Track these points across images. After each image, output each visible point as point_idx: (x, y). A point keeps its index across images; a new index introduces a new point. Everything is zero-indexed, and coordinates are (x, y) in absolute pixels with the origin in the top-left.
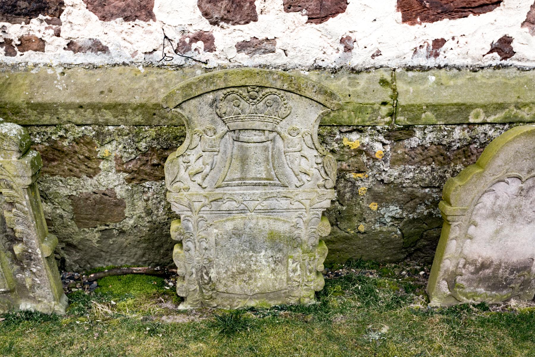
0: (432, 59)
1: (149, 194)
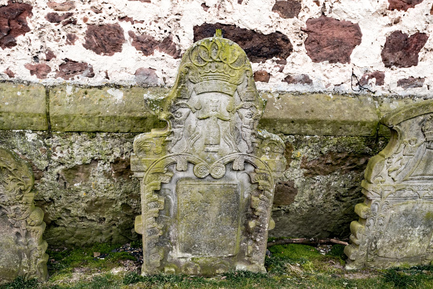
1: (316, 185)
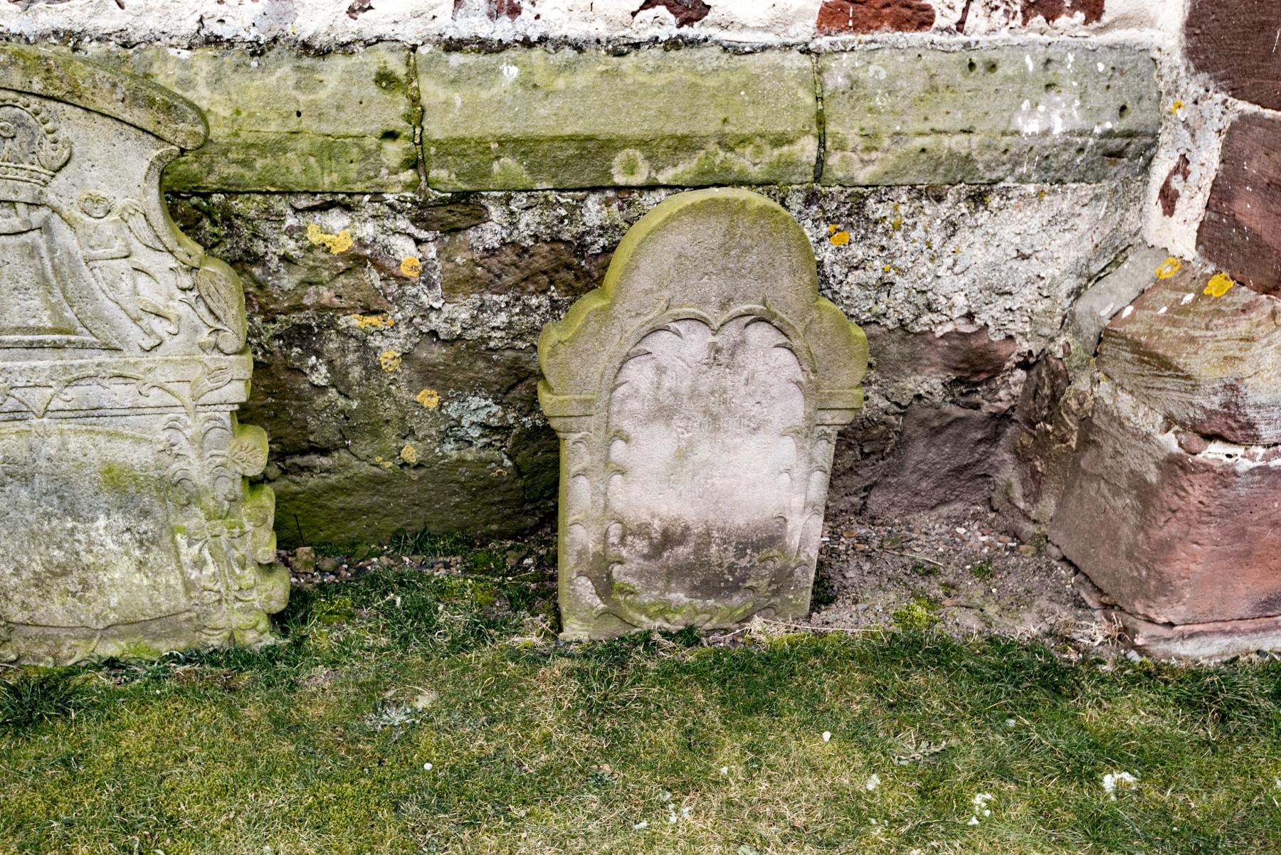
0: (505, 20)
